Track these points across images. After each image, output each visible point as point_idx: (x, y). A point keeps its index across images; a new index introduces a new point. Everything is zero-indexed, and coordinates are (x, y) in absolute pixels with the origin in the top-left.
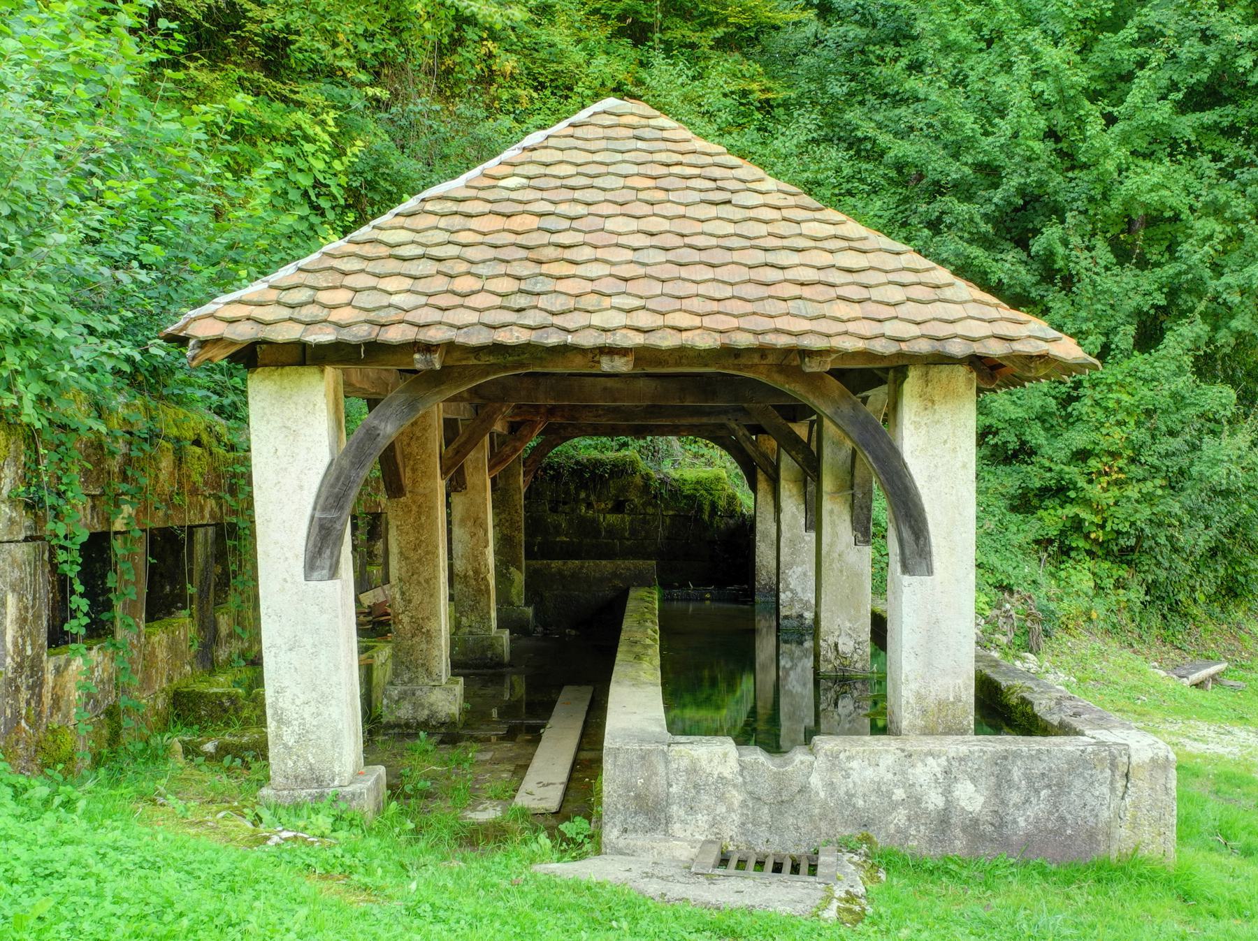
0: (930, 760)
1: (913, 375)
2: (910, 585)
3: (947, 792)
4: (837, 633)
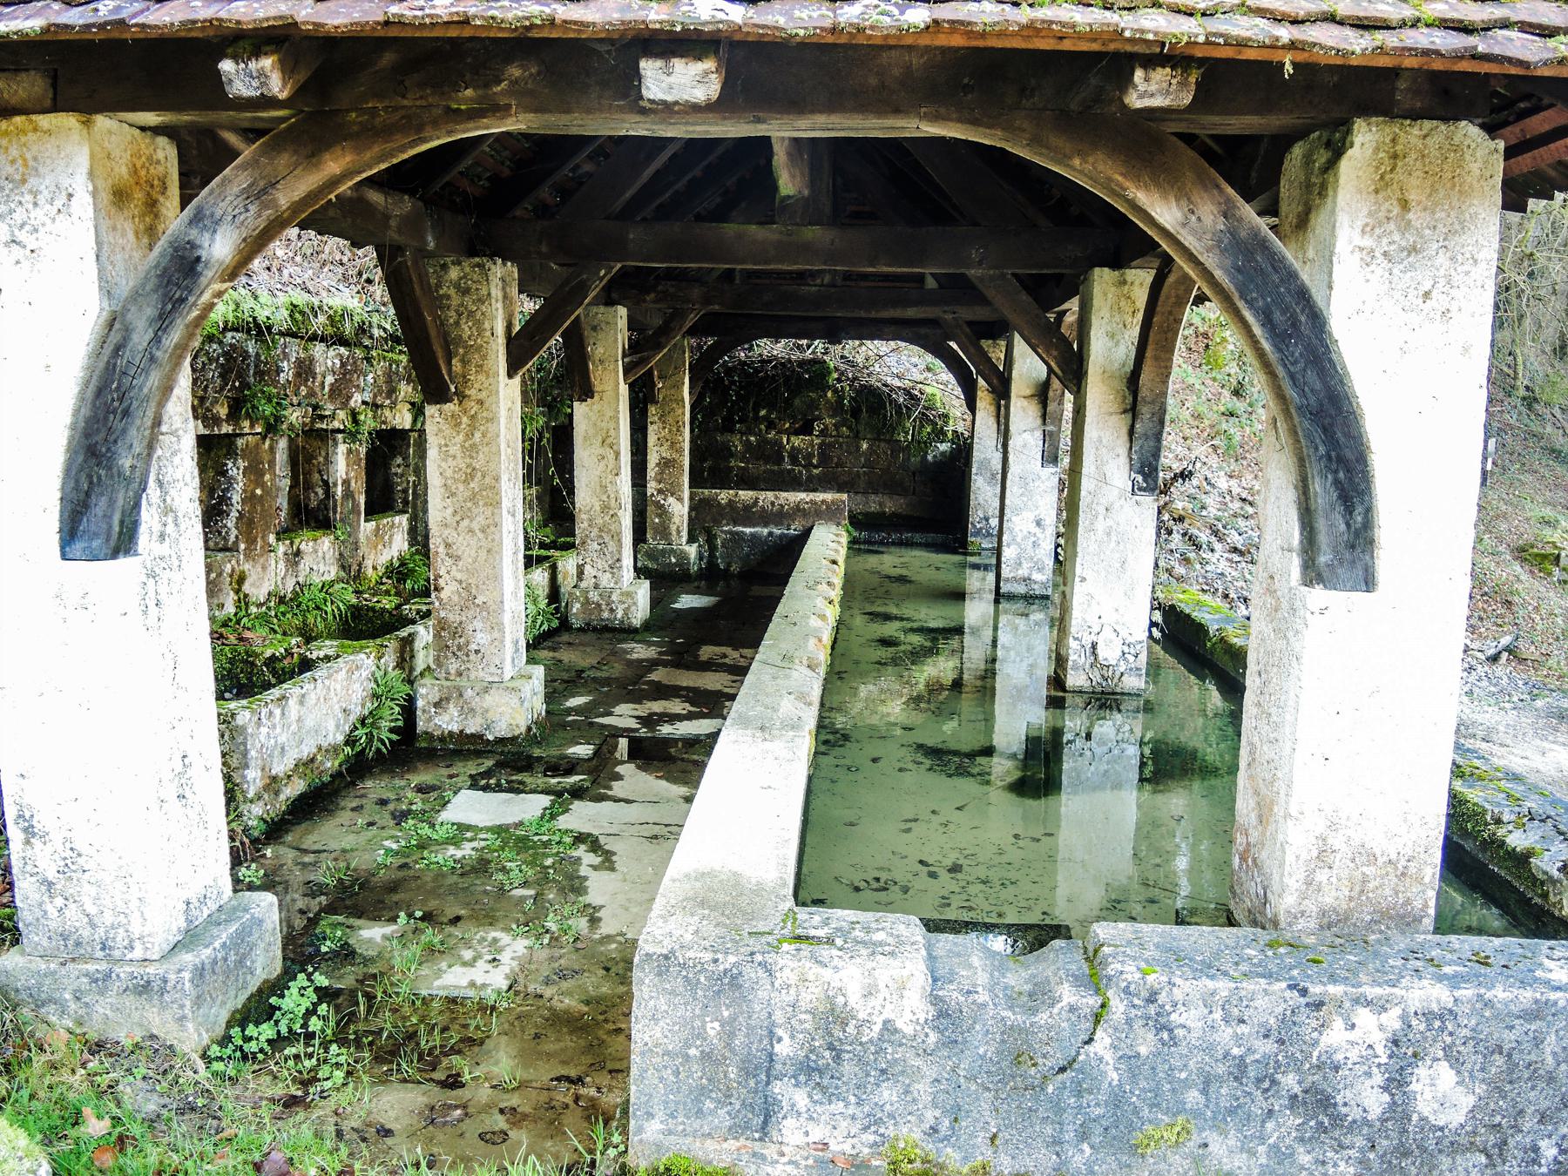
0: (1364, 1016)
3: (1396, 1082)
4: (1096, 629)
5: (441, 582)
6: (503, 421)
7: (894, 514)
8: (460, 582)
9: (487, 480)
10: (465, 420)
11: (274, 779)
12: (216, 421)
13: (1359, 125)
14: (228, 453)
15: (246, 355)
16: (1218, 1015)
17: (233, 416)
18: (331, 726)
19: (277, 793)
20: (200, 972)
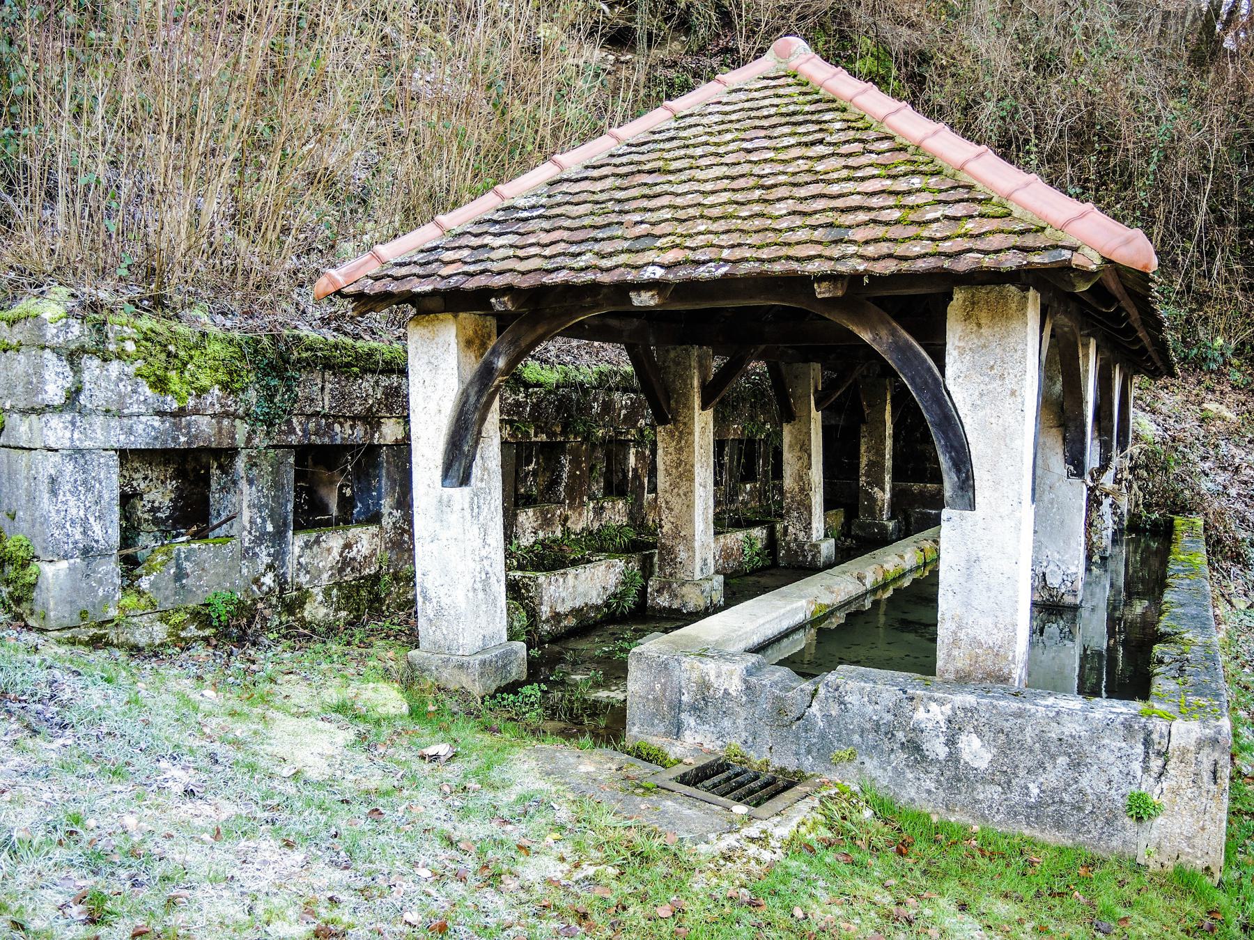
0: (933, 707)
1: (959, 296)
2: (949, 519)
3: (951, 742)
4: (1045, 564)
6: (697, 434)
11: (558, 614)
12: (555, 434)
13: (956, 290)
15: (571, 400)
16: (866, 699)
17: (564, 432)
18: (594, 594)
19: (559, 622)
20: (483, 663)
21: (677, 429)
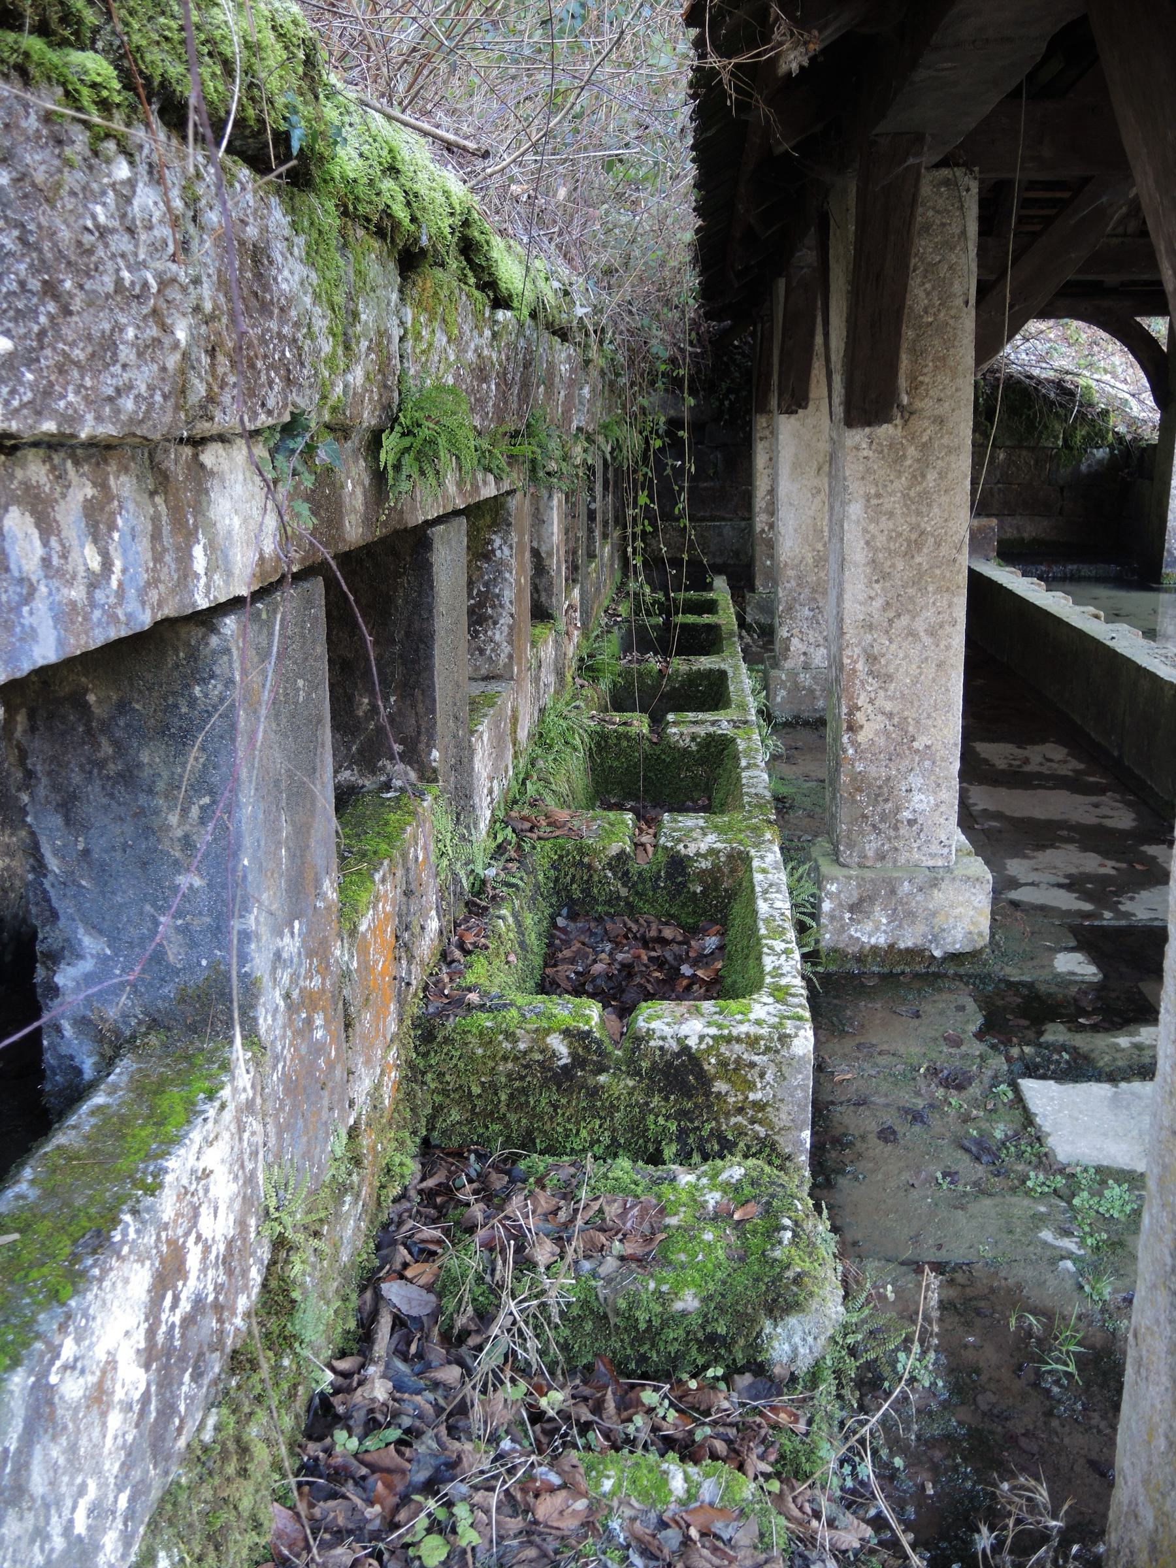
5: (860, 717)
7: (1035, 541)
8: (890, 716)
9: (944, 550)
10: (912, 451)
14: (494, 523)
21: (912, 438)
